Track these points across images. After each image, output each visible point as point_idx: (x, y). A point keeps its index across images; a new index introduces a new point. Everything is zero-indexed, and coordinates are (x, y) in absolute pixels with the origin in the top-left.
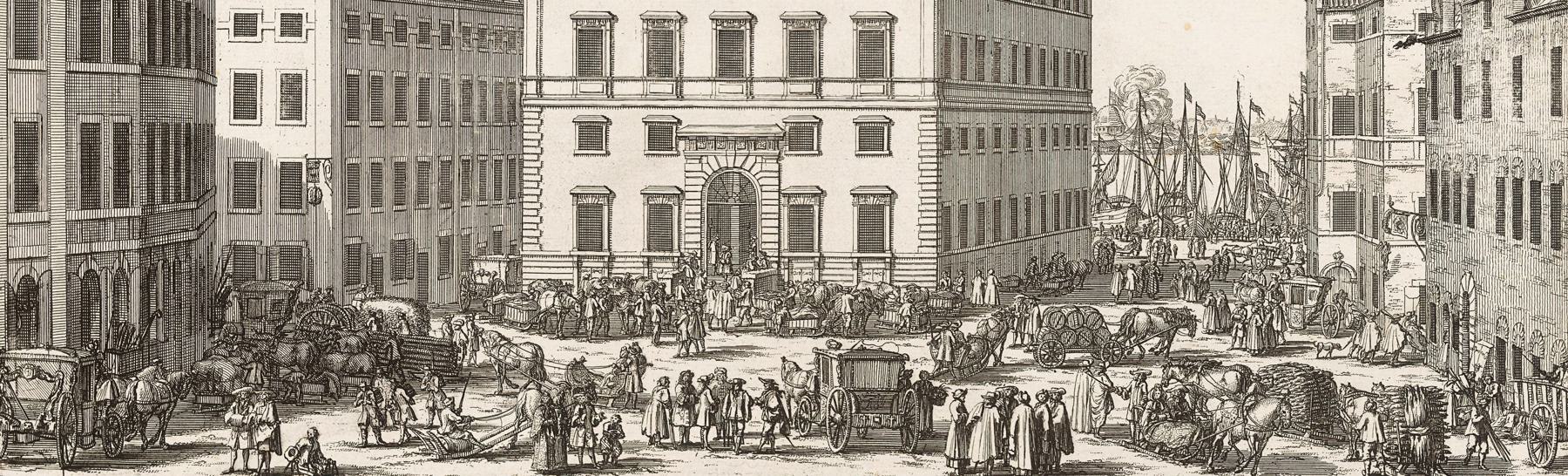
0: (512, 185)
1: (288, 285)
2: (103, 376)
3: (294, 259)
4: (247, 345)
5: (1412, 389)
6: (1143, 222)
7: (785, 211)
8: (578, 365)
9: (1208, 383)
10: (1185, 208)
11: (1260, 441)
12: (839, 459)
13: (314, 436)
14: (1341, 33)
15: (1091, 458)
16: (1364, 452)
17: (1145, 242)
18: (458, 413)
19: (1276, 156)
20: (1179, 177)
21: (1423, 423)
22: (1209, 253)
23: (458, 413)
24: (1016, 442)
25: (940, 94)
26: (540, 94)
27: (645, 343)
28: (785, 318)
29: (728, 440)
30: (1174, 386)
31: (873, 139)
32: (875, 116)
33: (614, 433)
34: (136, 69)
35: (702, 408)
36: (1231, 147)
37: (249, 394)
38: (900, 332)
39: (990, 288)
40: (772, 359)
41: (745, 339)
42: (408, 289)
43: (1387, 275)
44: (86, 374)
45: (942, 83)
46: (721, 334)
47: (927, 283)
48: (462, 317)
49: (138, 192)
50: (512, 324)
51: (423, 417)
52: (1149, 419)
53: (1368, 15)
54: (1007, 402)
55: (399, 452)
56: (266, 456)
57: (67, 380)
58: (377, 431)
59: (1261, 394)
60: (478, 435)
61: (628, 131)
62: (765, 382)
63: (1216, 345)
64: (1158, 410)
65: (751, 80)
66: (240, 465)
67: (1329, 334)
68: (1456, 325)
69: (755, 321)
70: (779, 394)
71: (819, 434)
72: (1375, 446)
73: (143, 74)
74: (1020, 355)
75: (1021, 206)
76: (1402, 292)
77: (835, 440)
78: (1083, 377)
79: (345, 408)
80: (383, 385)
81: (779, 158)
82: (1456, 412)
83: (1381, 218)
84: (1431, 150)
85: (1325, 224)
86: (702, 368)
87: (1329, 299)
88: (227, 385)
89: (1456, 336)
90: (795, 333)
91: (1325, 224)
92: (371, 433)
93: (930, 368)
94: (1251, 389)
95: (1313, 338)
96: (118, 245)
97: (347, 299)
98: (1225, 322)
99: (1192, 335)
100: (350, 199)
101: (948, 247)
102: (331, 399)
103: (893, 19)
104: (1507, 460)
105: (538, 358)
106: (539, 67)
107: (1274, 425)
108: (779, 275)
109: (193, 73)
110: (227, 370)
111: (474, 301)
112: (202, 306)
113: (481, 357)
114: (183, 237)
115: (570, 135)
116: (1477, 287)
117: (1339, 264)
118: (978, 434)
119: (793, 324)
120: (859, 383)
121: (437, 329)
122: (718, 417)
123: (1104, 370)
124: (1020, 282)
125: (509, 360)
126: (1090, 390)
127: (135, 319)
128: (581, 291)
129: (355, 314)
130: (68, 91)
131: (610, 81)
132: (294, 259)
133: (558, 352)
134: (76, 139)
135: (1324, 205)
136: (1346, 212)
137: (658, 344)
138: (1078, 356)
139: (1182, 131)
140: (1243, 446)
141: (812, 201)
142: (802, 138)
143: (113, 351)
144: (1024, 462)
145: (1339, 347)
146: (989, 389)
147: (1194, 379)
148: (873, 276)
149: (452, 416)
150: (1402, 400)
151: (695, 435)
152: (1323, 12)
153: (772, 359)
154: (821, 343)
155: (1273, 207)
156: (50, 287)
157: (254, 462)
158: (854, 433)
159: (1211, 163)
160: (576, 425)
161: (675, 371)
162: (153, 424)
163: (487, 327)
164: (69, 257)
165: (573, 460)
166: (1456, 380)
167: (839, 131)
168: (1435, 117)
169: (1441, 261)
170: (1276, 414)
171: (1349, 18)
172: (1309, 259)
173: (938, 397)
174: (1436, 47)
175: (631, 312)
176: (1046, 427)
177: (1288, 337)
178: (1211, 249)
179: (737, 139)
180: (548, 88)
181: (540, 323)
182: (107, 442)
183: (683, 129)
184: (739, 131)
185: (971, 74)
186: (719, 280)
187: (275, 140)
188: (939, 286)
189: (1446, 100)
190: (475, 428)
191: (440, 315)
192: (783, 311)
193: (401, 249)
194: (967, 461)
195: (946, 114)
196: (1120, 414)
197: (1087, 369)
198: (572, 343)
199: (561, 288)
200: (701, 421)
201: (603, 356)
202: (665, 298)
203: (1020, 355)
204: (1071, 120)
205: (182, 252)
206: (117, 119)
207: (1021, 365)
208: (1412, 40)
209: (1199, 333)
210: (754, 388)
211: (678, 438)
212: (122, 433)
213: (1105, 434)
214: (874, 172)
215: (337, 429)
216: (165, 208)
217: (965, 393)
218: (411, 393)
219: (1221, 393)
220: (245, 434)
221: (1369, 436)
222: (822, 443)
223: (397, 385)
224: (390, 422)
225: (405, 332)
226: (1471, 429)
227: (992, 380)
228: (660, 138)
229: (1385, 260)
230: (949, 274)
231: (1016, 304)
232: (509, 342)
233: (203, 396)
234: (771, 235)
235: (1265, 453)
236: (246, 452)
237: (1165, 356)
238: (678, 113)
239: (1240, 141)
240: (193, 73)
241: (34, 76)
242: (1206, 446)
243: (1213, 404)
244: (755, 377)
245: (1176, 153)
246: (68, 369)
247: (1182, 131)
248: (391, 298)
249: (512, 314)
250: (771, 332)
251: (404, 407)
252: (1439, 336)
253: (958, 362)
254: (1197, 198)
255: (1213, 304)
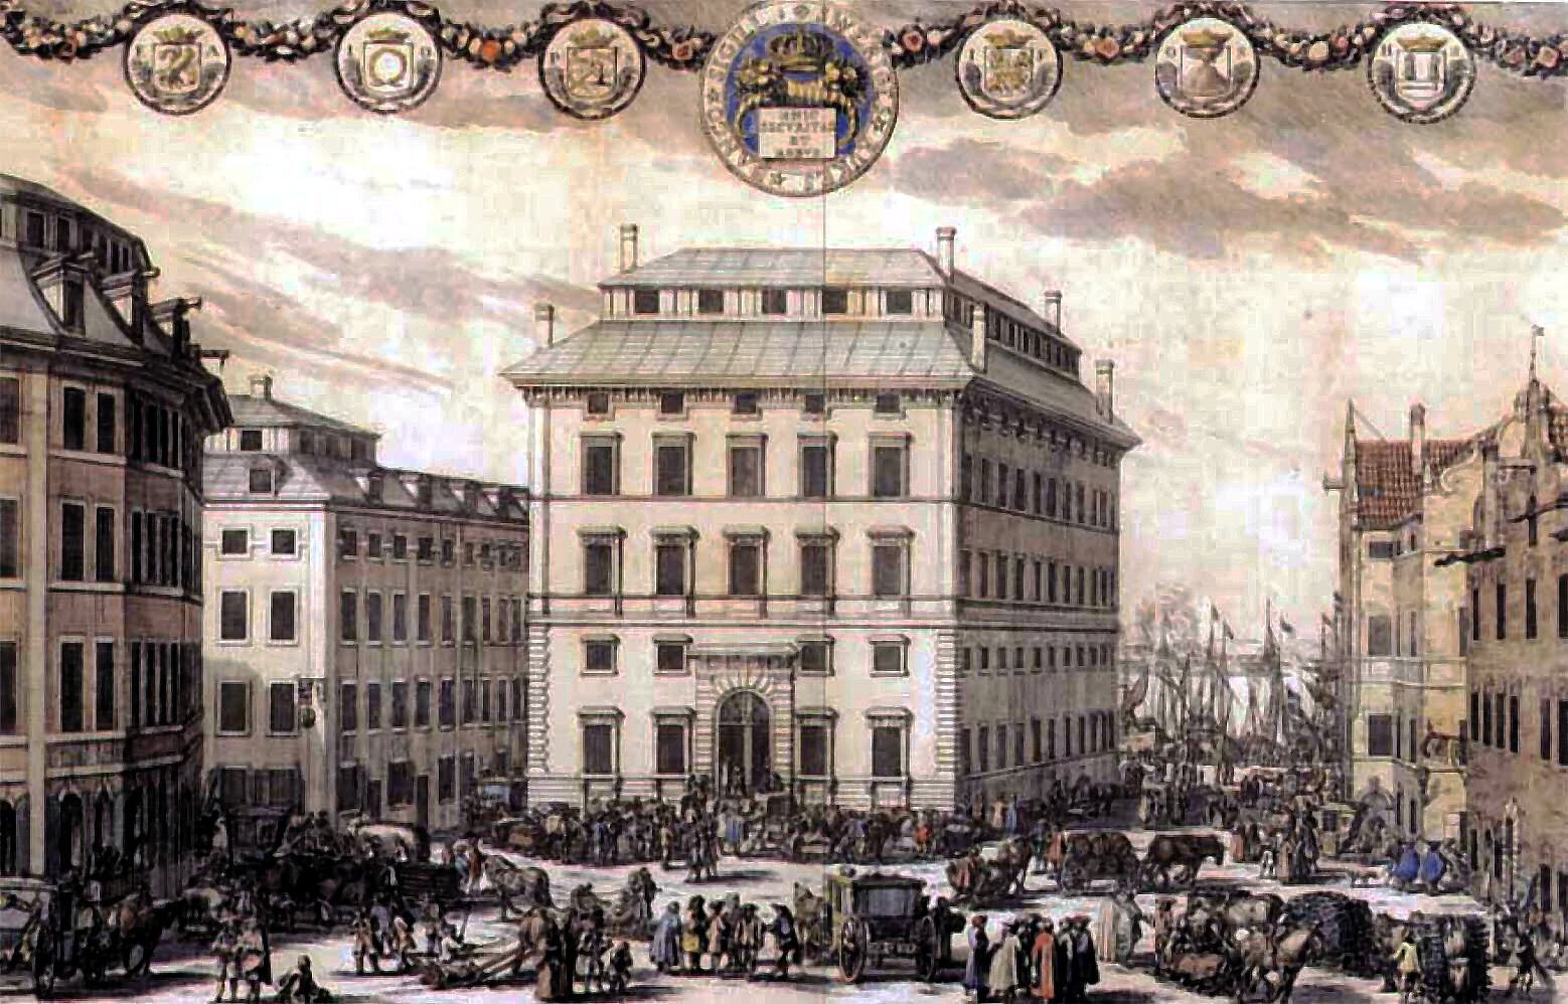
0: (516, 706)
1: (276, 811)
2: (86, 903)
3: (292, 783)
4: (235, 871)
5: (1452, 919)
6: (1167, 747)
7: (798, 733)
8: (583, 892)
9: (1237, 913)
10: (1212, 731)
11: (1291, 972)
12: (851, 989)
13: (305, 966)
14: (1380, 551)
15: (1117, 987)
16: (1401, 983)
17: (1169, 767)
18: (459, 940)
19: (1309, 677)
20: (1206, 699)
21: (1463, 954)
22: (1237, 778)
23: (459, 940)
24: (1039, 971)
25: (959, 612)
26: (546, 612)
27: (655, 869)
28: (799, 843)
29: (740, 966)
30: (1200, 916)
31: (888, 658)
32: (890, 635)
33: (623, 960)
34: (120, 587)
35: (713, 934)
36: (1261, 670)
37: (237, 923)
38: (916, 858)
39: (1012, 813)
40: (777, 886)
41: (761, 865)
42: (407, 813)
43: (1426, 802)
44: (66, 901)
45: (961, 602)
46: (734, 858)
47: (947, 807)
48: (464, 842)
49: (123, 716)
50: (517, 849)
51: (422, 946)
52: (1173, 948)
53: (1405, 534)
54: (1030, 931)
55: (397, 981)
56: (255, 987)
57: (46, 908)
58: (374, 959)
59: (1292, 925)
60: (478, 962)
61: (637, 652)
62: (776, 907)
63: (1244, 874)
64: (1183, 940)
65: (765, 598)
66: (227, 995)
67: (1364, 862)
68: (1498, 853)
69: (770, 845)
70: (791, 921)
71: (832, 962)
72: (1412, 977)
73: (128, 592)
74: (1043, 881)
75: (1045, 728)
76: (1441, 822)
77: (849, 971)
78: (1110, 905)
79: (339, 935)
80: (379, 911)
81: (792, 678)
82: (1498, 942)
83: (1420, 741)
84: (1472, 668)
85: (1360, 747)
86: (713, 893)
87: (1364, 825)
88: (214, 914)
89: (1498, 862)
90: (809, 859)
91: (1360, 747)
92: (366, 959)
93: (949, 893)
94: (1281, 919)
95: (1347, 866)
96: (101, 769)
97: (342, 822)
98: (1254, 850)
99: (1219, 862)
100: (347, 720)
101: (968, 770)
102: (323, 929)
103: (911, 535)
104: (1551, 992)
105: (542, 880)
106: (546, 582)
107: (1303, 957)
108: (792, 798)
109: (178, 592)
110: (215, 898)
111: (477, 824)
112: (191, 829)
113: (484, 883)
114: (168, 760)
115: (649, 655)
116: (1521, 813)
117: (1376, 791)
118: (997, 962)
119: (805, 850)
120: (874, 910)
121: (437, 855)
122: (732, 945)
123: (1131, 897)
124: (1043, 806)
125: (513, 886)
126: (1117, 917)
127: (119, 843)
128: (588, 815)
129: (350, 839)
130: (48, 610)
131: (619, 598)
132: (292, 783)
133: (562, 878)
134: (57, 660)
135: (1360, 728)
136: (1381, 740)
137: (667, 868)
138: (1103, 882)
139: (1209, 652)
140: (1273, 976)
141: (827, 723)
142: (813, 657)
143: (96, 877)
144: (1047, 988)
145: (1374, 875)
146: (1010, 916)
147: (1221, 908)
148: (890, 797)
149: (453, 944)
150: (1442, 931)
151: (706, 962)
152: (1359, 529)
153: (777, 886)
154: (834, 869)
155: (1306, 732)
156: (27, 812)
157: (243, 991)
158: (868, 962)
159: (1239, 684)
160: (583, 952)
161: (685, 898)
162: (136, 954)
163: (491, 852)
164: (48, 782)
165: (578, 988)
166: (1498, 908)
167: (853, 655)
168: (1476, 636)
169: (1484, 785)
170: (1307, 945)
171: (1384, 536)
172: (1343, 785)
173: (958, 924)
174: (1476, 565)
175: (640, 837)
176: (1070, 954)
177: (1320, 863)
178: (1240, 773)
179: (750, 659)
180: (556, 606)
181: (545, 846)
182: (87, 973)
183: (694, 649)
184: (753, 651)
185: (992, 591)
186: (731, 804)
187: (264, 660)
188: (958, 811)
189: (1489, 621)
190: (477, 956)
191: (439, 840)
192: (795, 836)
193: (400, 774)
194: (987, 990)
195: (966, 633)
196: (1147, 943)
197: (1113, 895)
198: (578, 868)
199: (565, 811)
200: (712, 947)
201: (611, 883)
202: (675, 820)
203: (1043, 881)
204: (1101, 639)
205: (169, 775)
206: (101, 640)
207: (1043, 892)
208: (1452, 558)
209: (1227, 858)
210: (767, 914)
211: (688, 964)
212: (94, 962)
213: (1131, 961)
214: (890, 692)
215: (331, 957)
216: (149, 731)
217: (984, 920)
218: (410, 921)
219: (1249, 924)
220: (232, 964)
221: (1406, 966)
222: (834, 972)
223: (394, 913)
224: (387, 951)
225: (404, 859)
226: (1514, 959)
227: (1012, 907)
228: (670, 657)
229: (1423, 784)
230: (968, 797)
231: (1039, 830)
232: (512, 866)
233: (185, 928)
234: (783, 756)
235: (1297, 983)
236: (234, 983)
237: (1195, 889)
238: (688, 632)
239: (1270, 662)
240: (178, 592)
241: (13, 594)
242: (1232, 975)
243: (1241, 934)
244: (768, 903)
245: (1203, 674)
246: (45, 897)
247: (1209, 652)
248: (389, 823)
249: (516, 838)
250: (784, 857)
251: (403, 935)
252: (1481, 862)
253: (978, 888)
254: (1224, 722)
255: (1241, 830)
